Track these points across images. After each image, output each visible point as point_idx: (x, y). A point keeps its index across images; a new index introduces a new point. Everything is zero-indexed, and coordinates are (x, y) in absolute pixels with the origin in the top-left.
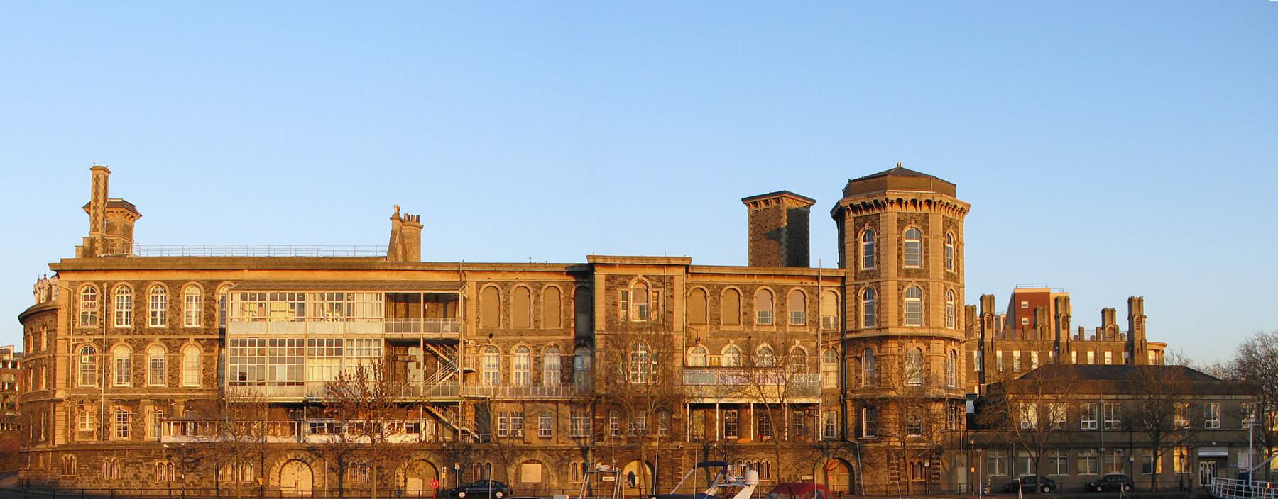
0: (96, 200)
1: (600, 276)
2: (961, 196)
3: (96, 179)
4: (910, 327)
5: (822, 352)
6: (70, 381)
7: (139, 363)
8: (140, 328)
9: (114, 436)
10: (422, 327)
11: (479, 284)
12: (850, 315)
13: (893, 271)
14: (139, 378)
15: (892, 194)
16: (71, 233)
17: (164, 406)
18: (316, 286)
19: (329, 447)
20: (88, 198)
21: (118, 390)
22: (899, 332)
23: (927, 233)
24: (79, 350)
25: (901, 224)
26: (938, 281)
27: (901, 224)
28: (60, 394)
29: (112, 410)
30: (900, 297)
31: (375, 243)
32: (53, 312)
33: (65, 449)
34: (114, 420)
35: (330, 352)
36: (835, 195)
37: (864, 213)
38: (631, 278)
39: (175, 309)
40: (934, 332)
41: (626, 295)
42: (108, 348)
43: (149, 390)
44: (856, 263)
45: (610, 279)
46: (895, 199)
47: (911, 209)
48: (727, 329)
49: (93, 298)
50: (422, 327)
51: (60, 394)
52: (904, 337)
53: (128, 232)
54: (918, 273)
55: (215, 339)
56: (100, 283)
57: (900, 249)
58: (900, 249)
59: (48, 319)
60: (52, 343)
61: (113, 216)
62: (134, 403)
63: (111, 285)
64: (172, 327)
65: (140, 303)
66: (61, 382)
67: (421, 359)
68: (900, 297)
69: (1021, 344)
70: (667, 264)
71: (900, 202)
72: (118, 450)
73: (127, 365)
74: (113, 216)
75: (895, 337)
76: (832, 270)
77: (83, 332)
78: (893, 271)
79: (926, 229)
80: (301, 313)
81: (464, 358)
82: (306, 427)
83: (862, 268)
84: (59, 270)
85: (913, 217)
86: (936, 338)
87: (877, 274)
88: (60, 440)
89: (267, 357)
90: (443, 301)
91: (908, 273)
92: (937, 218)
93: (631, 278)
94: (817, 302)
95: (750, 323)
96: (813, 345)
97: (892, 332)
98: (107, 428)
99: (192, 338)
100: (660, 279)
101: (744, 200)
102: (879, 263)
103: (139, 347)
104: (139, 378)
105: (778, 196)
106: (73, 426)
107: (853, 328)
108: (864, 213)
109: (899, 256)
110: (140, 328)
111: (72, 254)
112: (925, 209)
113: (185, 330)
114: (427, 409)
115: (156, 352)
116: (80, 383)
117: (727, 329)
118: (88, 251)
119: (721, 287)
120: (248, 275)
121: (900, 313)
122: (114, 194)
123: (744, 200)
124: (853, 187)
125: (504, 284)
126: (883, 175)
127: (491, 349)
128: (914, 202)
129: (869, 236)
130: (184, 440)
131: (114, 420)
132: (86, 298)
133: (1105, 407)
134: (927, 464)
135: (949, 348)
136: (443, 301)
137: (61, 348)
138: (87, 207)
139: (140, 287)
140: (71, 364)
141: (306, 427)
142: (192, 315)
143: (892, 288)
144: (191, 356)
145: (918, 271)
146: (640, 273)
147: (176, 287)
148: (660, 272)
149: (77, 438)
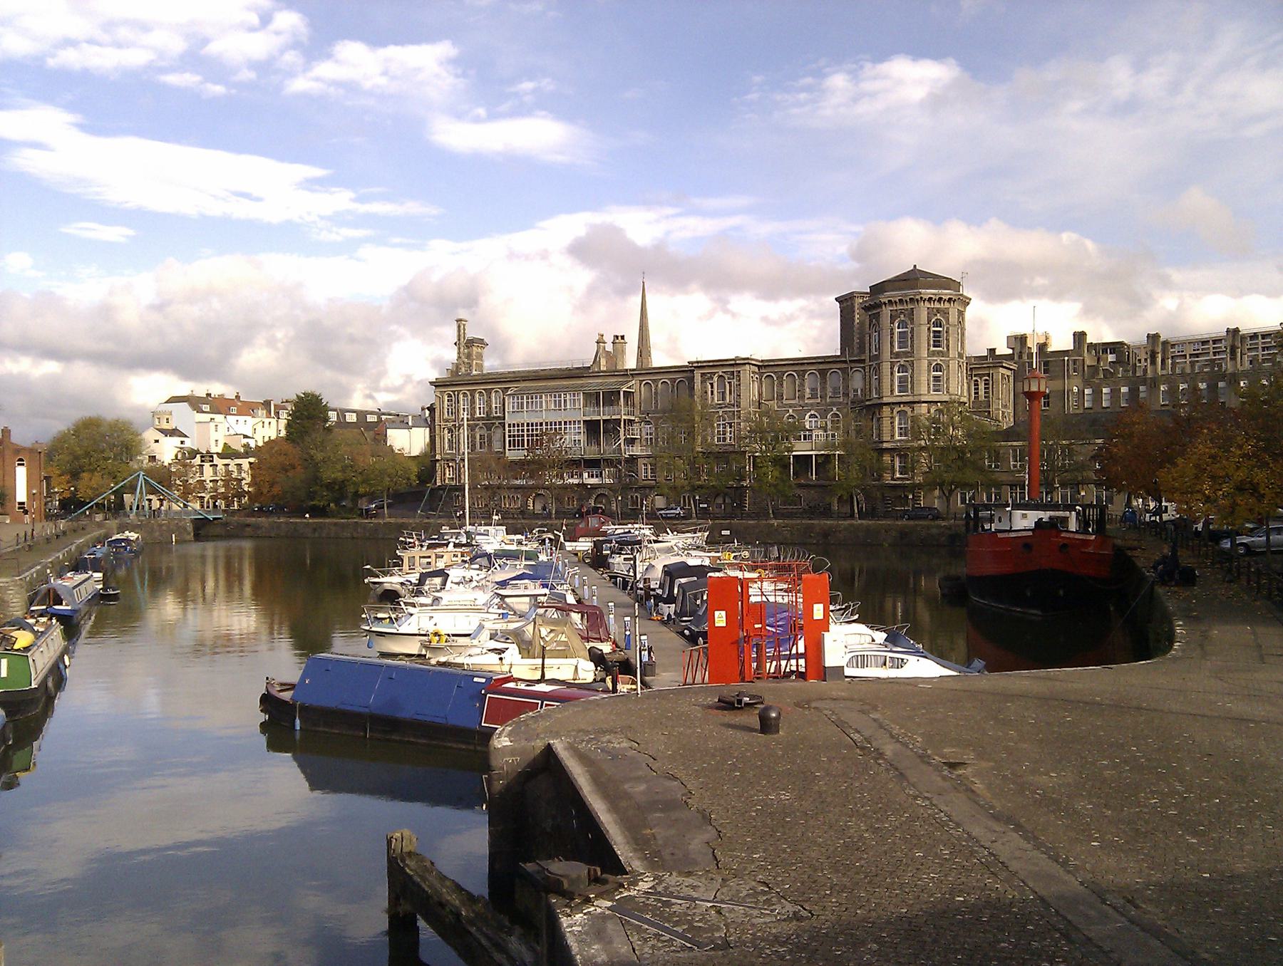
1: (697, 374)
6: (443, 448)
11: (703, 374)
13: (886, 355)
26: (954, 359)
28: (438, 457)
30: (929, 371)
40: (916, 399)
44: (892, 346)
45: (703, 374)
47: (937, 305)
50: (602, 415)
51: (438, 457)
54: (906, 354)
71: (940, 299)
77: (447, 421)
82: (586, 475)
83: (897, 349)
84: (437, 384)
87: (911, 354)
90: (611, 397)
91: (898, 355)
92: (953, 310)
95: (802, 397)
97: (885, 400)
102: (912, 346)
111: (445, 375)
112: (947, 305)
114: (610, 463)
118: (455, 371)
122: (471, 334)
127: (648, 423)
136: (611, 397)
141: (586, 475)
143: (886, 367)
147: (489, 391)
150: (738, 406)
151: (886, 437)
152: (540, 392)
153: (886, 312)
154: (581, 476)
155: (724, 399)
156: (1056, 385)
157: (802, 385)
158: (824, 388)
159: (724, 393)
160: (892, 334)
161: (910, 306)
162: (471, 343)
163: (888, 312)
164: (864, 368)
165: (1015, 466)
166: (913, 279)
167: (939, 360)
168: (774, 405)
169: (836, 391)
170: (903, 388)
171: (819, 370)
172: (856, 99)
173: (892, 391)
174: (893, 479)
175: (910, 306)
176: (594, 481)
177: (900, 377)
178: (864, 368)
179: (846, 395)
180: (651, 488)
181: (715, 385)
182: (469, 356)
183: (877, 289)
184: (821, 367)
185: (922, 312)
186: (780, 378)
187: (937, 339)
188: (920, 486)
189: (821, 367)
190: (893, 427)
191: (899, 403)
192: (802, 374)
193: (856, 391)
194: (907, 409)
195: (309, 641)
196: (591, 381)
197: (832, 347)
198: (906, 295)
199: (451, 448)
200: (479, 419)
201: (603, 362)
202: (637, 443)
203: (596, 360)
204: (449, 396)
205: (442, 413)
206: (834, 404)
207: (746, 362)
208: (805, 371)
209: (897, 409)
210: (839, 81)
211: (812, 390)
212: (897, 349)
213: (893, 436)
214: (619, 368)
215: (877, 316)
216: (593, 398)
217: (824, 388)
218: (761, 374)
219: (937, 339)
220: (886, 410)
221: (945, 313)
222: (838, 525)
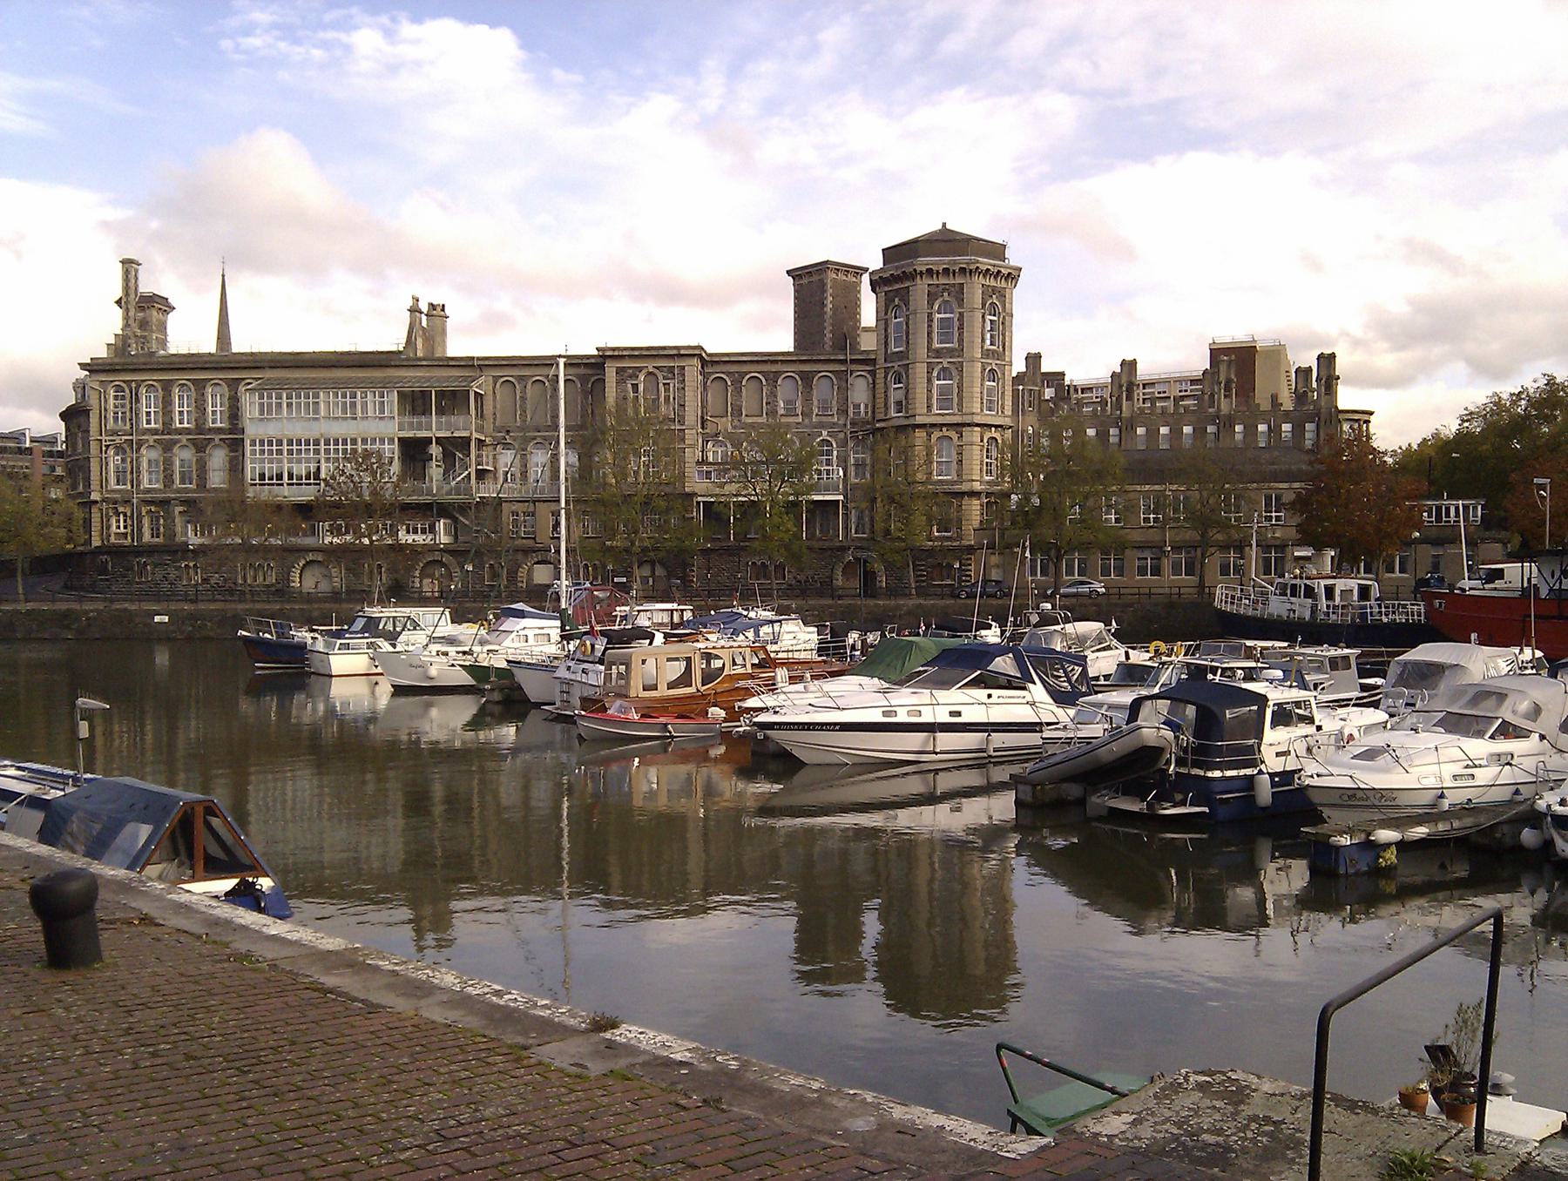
0: (127, 294)
2: (1013, 258)
3: (126, 273)
4: (937, 415)
5: (851, 444)
6: (103, 482)
7: (168, 464)
8: (167, 428)
9: (147, 537)
10: (435, 427)
12: (880, 401)
13: (922, 352)
14: (168, 479)
16: (101, 329)
17: (191, 506)
19: (343, 550)
20: (119, 294)
21: (149, 491)
23: (961, 306)
24: (111, 452)
27: (932, 298)
30: (929, 380)
31: (389, 336)
32: (87, 412)
33: (99, 551)
34: (146, 522)
36: (875, 262)
38: (640, 369)
39: (201, 408)
40: (967, 419)
41: (635, 387)
42: (138, 450)
43: (178, 491)
44: (983, 340)
45: (619, 371)
46: (924, 269)
47: (943, 281)
48: (750, 420)
49: (123, 398)
50: (435, 427)
51: (95, 496)
53: (163, 327)
54: (950, 352)
55: (234, 442)
57: (930, 326)
58: (930, 326)
59: (82, 419)
60: (87, 445)
61: (143, 309)
62: (164, 503)
65: (167, 403)
66: (95, 484)
67: (1521, 657)
68: (929, 380)
70: (678, 353)
71: (930, 272)
72: (151, 550)
73: (157, 465)
74: (143, 309)
76: (788, 353)
78: (922, 352)
79: (961, 301)
80: (316, 411)
84: (93, 367)
85: (946, 288)
86: (969, 425)
87: (960, 351)
88: (96, 542)
90: (453, 400)
92: (975, 290)
93: (640, 369)
94: (844, 391)
95: (772, 413)
96: (842, 435)
97: (919, 420)
98: (140, 529)
99: (217, 438)
102: (961, 341)
103: (167, 447)
104: (168, 479)
105: (823, 267)
106: (109, 527)
107: (882, 416)
108: (943, 281)
109: (929, 334)
110: (167, 428)
113: (210, 429)
114: (443, 510)
115: (183, 456)
116: (113, 485)
117: (750, 420)
118: (120, 346)
119: (778, 374)
120: (269, 374)
121: (929, 399)
122: (145, 287)
124: (890, 254)
125: (521, 378)
127: (507, 446)
128: (946, 271)
130: (608, 1035)
131: (146, 522)
132: (116, 398)
133: (380, 424)
134: (957, 566)
137: (94, 447)
138: (119, 302)
140: (104, 464)
142: (216, 416)
143: (920, 370)
144: (218, 459)
145: (952, 350)
146: (650, 365)
147: (200, 385)
149: (113, 539)
152: (315, 386)
153: (921, 287)
154: (432, 530)
157: (773, 394)
158: (807, 400)
160: (930, 320)
161: (959, 280)
163: (428, 321)
164: (873, 373)
165: (1147, 520)
166: (946, 241)
169: (825, 407)
170: (945, 402)
171: (800, 373)
172: (393, 68)
173: (929, 407)
175: (959, 280)
178: (873, 373)
179: (843, 411)
180: (527, 552)
181: (641, 387)
182: (144, 324)
184: (807, 368)
186: (737, 383)
188: (970, 549)
189: (807, 368)
192: (773, 378)
197: (783, 340)
198: (955, 262)
200: (180, 432)
203: (410, 341)
204: (119, 389)
205: (102, 418)
206: (822, 425)
207: (696, 353)
208: (778, 374)
209: (936, 434)
210: (367, 40)
211: (787, 402)
212: (936, 345)
214: (438, 355)
215: (904, 295)
216: (415, 403)
217: (807, 400)
222: (898, 607)
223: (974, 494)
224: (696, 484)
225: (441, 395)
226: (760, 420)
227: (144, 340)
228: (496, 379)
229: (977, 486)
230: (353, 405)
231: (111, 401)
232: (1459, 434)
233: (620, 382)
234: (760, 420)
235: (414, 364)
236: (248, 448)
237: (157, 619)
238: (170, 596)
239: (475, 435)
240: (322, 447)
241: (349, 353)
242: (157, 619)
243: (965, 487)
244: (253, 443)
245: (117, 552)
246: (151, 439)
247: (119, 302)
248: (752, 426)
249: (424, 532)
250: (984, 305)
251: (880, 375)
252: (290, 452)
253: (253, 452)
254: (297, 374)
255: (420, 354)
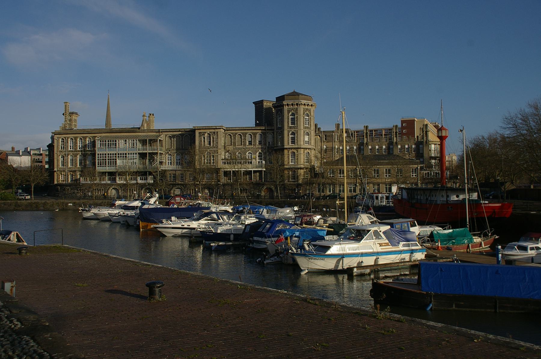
1: (197, 132)
5: (267, 154)
6: (58, 165)
11: (200, 133)
13: (302, 127)
15: (285, 103)
18: (121, 138)
21: (70, 168)
22: (287, 147)
25: (289, 112)
27: (289, 112)
29: (69, 174)
30: (288, 135)
34: (70, 176)
35: (123, 157)
37: (291, 107)
45: (200, 133)
48: (238, 147)
50: (148, 150)
52: (289, 148)
56: (65, 137)
63: (77, 137)
64: (84, 150)
68: (288, 135)
69: (379, 144)
71: (288, 105)
75: (287, 149)
77: (61, 152)
78: (302, 127)
81: (158, 158)
84: (55, 133)
88: (56, 182)
89: (107, 158)
91: (291, 128)
95: (245, 145)
100: (214, 133)
101: (253, 103)
102: (297, 124)
107: (275, 145)
109: (288, 122)
117: (238, 147)
118: (64, 128)
121: (288, 141)
122: (71, 110)
123: (253, 103)
124: (277, 99)
126: (284, 96)
128: (292, 105)
129: (293, 114)
131: (70, 176)
135: (306, 151)
136: (152, 141)
138: (63, 114)
139: (76, 138)
143: (286, 132)
146: (208, 131)
148: (213, 131)
150: (217, 148)
151: (286, 163)
155: (210, 144)
156: (330, 145)
159: (210, 142)
160: (288, 118)
162: (72, 113)
164: (273, 133)
167: (307, 130)
168: (231, 148)
170: (293, 142)
174: (289, 181)
176: (143, 182)
177: (292, 137)
182: (70, 120)
183: (280, 99)
185: (301, 109)
187: (293, 121)
190: (289, 159)
191: (292, 148)
193: (269, 143)
194: (295, 151)
195: (356, 276)
196: (140, 134)
199: (63, 165)
201: (145, 125)
202: (167, 163)
208: (236, 134)
209: (291, 151)
213: (289, 163)
216: (144, 142)
218: (226, 134)
219: (293, 121)
220: (286, 151)
221: (310, 111)
223: (301, 168)
224: (220, 165)
225: (150, 140)
226: (241, 147)
227: (70, 125)
228: (166, 135)
229: (302, 166)
230: (116, 144)
231: (60, 142)
232: (31, 166)
233: (200, 136)
234: (241, 147)
235: (144, 131)
236: (97, 156)
237: (69, 204)
238: (72, 198)
239: (159, 152)
240: (117, 156)
241: (125, 129)
242: (69, 204)
243: (299, 166)
244: (98, 154)
245: (61, 185)
246: (71, 153)
247: (63, 114)
248: (239, 149)
249: (145, 180)
250: (304, 114)
251: (275, 133)
252: (118, 157)
253: (98, 157)
254: (275, 137)
255: (145, 128)
